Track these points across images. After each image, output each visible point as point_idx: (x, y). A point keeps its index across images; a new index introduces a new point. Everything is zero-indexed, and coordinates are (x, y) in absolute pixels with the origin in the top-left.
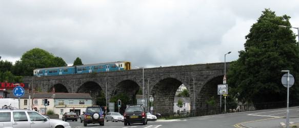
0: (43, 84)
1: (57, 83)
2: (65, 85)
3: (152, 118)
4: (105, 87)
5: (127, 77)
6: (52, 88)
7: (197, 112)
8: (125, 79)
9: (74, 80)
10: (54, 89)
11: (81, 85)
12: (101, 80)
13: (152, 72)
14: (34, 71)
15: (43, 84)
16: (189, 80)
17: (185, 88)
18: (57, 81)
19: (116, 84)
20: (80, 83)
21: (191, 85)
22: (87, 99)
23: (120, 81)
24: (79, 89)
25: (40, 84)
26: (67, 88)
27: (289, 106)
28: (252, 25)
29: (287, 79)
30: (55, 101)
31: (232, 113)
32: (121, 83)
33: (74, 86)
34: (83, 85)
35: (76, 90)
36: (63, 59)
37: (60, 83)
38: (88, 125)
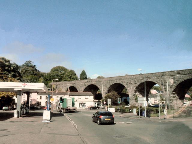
0: (63, 87)
1: (71, 86)
2: (76, 87)
3: (17, 114)
4: (102, 88)
5: (117, 81)
6: (68, 89)
8: (115, 82)
9: (82, 84)
10: (69, 89)
12: (91, 81)
13: (134, 77)
15: (63, 87)
16: (164, 82)
17: (5, 68)
20: (85, 86)
21: (165, 86)
23: (112, 84)
27: (140, 115)
31: (128, 113)
34: (87, 87)
36: (51, 69)
37: (73, 86)
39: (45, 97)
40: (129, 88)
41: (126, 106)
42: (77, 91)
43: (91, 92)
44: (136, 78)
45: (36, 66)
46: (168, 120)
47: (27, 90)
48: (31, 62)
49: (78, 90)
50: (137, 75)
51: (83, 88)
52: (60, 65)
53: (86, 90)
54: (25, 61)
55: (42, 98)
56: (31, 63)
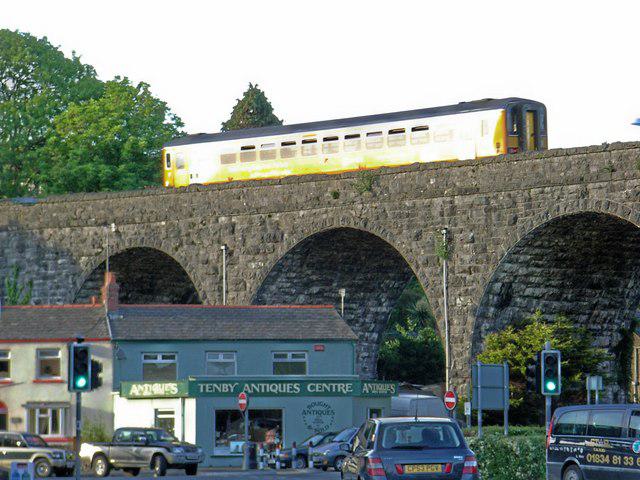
5: (585, 194)
18: (129, 231)
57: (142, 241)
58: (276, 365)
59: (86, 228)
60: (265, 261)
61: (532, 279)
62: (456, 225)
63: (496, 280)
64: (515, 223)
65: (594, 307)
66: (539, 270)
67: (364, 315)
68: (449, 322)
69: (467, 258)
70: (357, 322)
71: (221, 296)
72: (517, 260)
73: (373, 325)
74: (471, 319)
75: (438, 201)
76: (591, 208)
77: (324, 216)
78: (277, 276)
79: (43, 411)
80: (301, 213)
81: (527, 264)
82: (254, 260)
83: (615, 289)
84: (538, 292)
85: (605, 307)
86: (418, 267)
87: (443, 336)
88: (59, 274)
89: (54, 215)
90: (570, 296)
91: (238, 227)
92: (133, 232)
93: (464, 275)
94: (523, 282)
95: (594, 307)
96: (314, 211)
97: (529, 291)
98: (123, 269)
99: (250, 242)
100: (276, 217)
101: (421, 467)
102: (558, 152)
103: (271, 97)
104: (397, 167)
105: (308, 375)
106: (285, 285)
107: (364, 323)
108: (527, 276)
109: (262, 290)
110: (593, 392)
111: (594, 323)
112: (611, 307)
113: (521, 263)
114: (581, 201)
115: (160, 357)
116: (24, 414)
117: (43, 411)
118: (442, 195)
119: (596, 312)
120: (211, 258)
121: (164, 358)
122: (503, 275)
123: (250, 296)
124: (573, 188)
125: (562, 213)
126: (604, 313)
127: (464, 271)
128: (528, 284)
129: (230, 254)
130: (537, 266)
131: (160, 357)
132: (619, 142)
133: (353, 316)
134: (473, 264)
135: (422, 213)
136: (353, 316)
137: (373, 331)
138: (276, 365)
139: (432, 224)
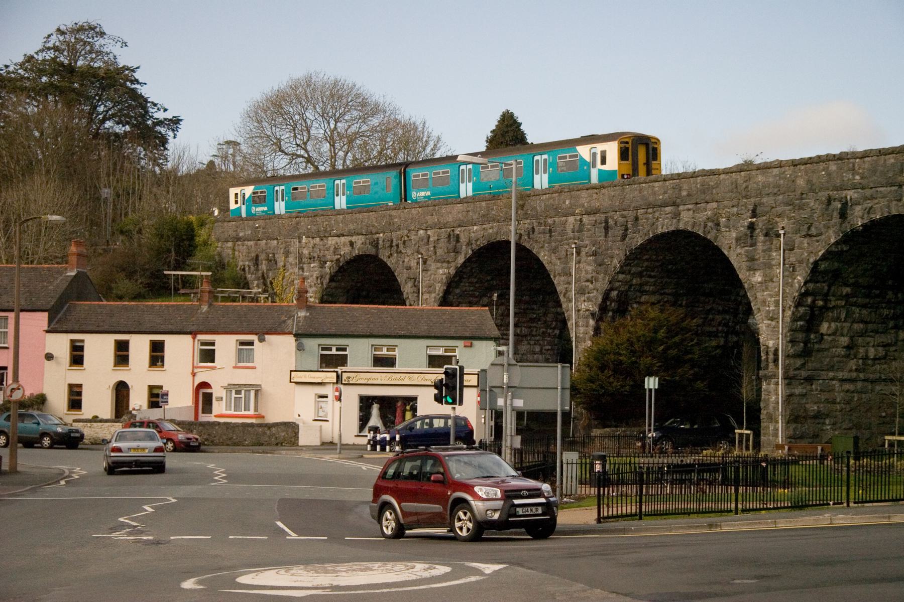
2: (391, 263)
5: (677, 215)
7: (51, 447)
8: (665, 225)
11: (461, 260)
14: (233, 191)
18: (359, 240)
19: (617, 256)
22: (470, 338)
24: (452, 284)
25: (287, 254)
26: (401, 277)
28: (501, 114)
29: (509, 378)
30: (300, 348)
32: (643, 248)
33: (433, 266)
34: (468, 260)
35: (439, 288)
38: (55, 446)
39: (313, 397)
40: (758, 278)
41: (266, 209)
42: (404, 304)
43: (489, 304)
44: (812, 190)
45: (137, 75)
46: (309, 201)
47: (528, 488)
48: (102, 34)
49: (407, 289)
50: (819, 160)
51: (441, 273)
52: (299, 73)
53: (465, 286)
54: (52, 29)
55: (88, 355)
56: (99, 42)
57: (668, 228)
58: (323, 357)
59: (330, 238)
60: (448, 268)
61: (647, 288)
62: (582, 241)
63: (612, 289)
64: (625, 239)
65: (708, 312)
66: (652, 280)
67: (545, 314)
68: (576, 323)
69: (590, 268)
70: (539, 320)
71: (418, 296)
72: (630, 271)
73: (554, 323)
74: (592, 322)
75: (571, 219)
76: (681, 226)
77: (491, 231)
78: (460, 281)
79: (238, 392)
80: (475, 228)
81: (640, 275)
82: (442, 267)
83: (727, 297)
84: (653, 299)
85: (719, 313)
86: (555, 276)
87: (571, 336)
88: (312, 276)
89: (309, 227)
90: (684, 302)
91: (431, 239)
92: (361, 242)
93: (588, 284)
94: (639, 291)
95: (708, 312)
96: (484, 226)
97: (643, 299)
98: (361, 272)
99: (440, 252)
100: (457, 231)
101: (853, 478)
102: (665, 179)
103: (492, 130)
104: (888, 149)
105: (397, 368)
106: (468, 288)
107: (545, 322)
108: (641, 285)
109: (447, 293)
110: (650, 390)
111: (710, 325)
112: (725, 312)
113: (634, 274)
114: (674, 221)
115: (334, 349)
116: (223, 394)
117: (238, 392)
118: (574, 214)
119: (711, 316)
120: (412, 265)
121: (337, 350)
122: (617, 284)
123: (438, 297)
124: (668, 209)
125: (659, 231)
126: (719, 318)
127: (587, 281)
128: (643, 292)
129: (425, 262)
130: (650, 276)
131: (334, 349)
132: (704, 170)
133: (535, 316)
134: (594, 274)
135: (559, 229)
136: (535, 316)
137: (554, 328)
138: (323, 357)
139: (566, 239)
